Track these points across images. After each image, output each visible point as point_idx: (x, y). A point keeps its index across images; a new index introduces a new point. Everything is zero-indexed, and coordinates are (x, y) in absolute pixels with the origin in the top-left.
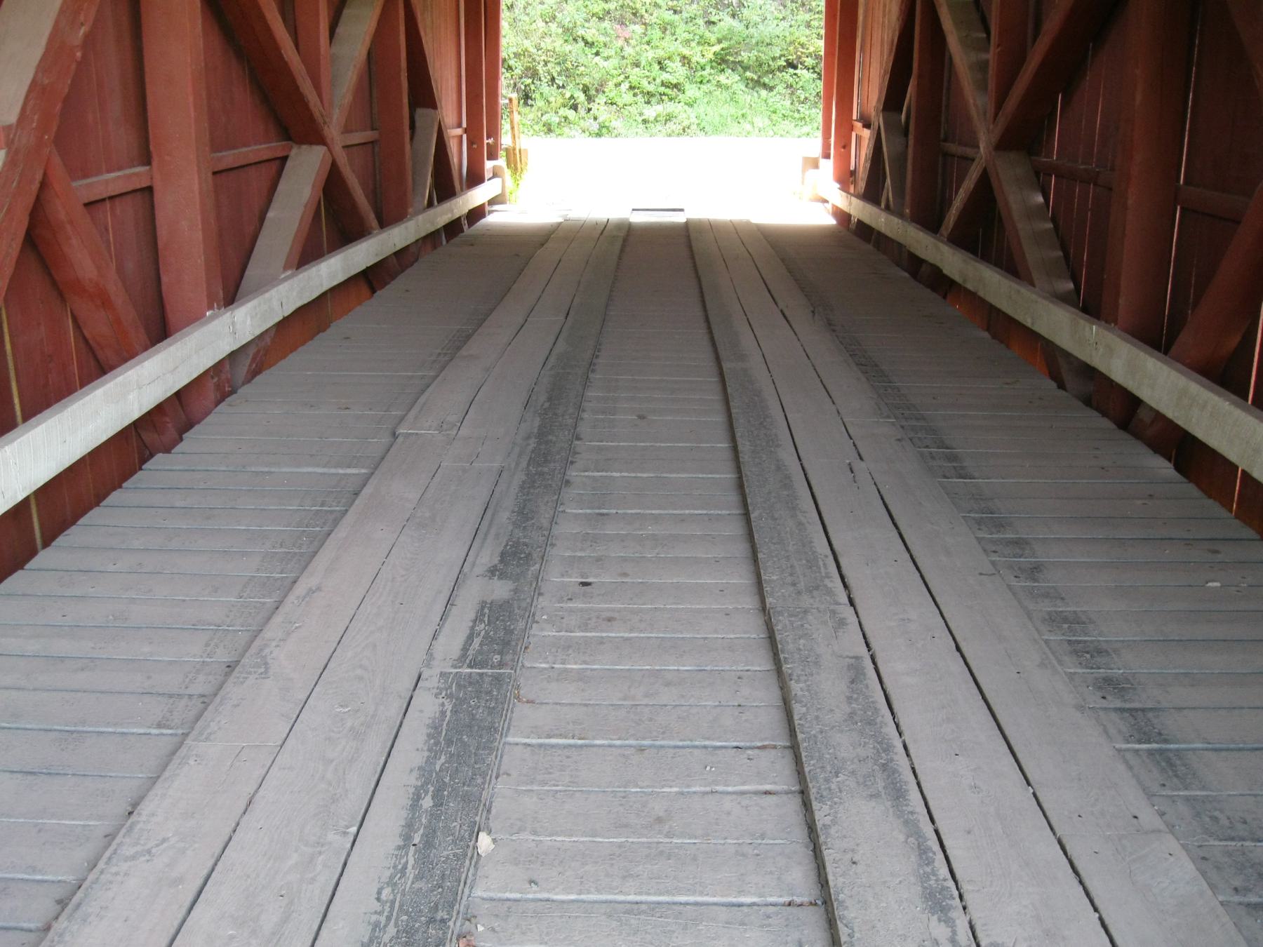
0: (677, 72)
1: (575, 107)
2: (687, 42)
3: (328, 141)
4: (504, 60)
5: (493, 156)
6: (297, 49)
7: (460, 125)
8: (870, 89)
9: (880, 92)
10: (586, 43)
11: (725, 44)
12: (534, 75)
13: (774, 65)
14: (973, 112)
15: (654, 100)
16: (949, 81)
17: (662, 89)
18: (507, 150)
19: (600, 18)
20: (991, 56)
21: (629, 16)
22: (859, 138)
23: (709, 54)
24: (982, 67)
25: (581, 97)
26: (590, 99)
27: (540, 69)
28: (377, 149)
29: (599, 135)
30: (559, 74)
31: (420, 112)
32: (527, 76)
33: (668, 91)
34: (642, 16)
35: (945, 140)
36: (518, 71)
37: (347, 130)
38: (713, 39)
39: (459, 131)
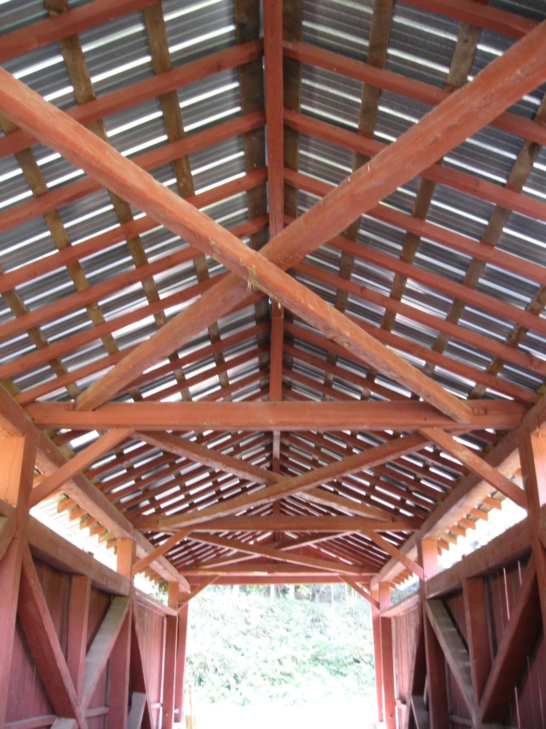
0: (289, 666)
1: (229, 687)
2: (295, 648)
3: (78, 716)
4: (188, 658)
5: (177, 720)
6: (67, 662)
7: (159, 701)
8: (403, 681)
9: (409, 681)
10: (236, 648)
11: (317, 649)
12: (205, 667)
13: (346, 661)
14: (465, 698)
15: (276, 683)
16: (450, 688)
17: (281, 676)
18: (187, 718)
19: (244, 634)
20: (471, 663)
21: (261, 632)
22: (400, 711)
23: (309, 654)
24: (467, 670)
25: (232, 682)
26: (238, 682)
27: (209, 663)
28: (107, 718)
29: (243, 704)
30: (220, 667)
31: (135, 695)
32: (201, 668)
33: (284, 677)
34: (268, 633)
35: (452, 713)
36: (195, 665)
37: (90, 707)
38: (310, 646)
39: (158, 706)
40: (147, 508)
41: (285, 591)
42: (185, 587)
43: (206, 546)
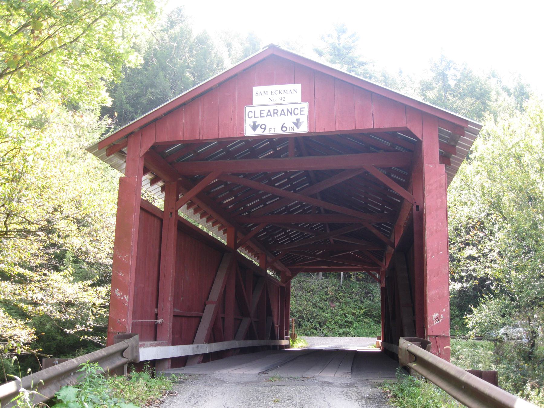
7: (278, 324)
12: (302, 318)
39: (277, 326)
40: (271, 241)
41: (350, 276)
42: (288, 273)
43: (295, 255)
